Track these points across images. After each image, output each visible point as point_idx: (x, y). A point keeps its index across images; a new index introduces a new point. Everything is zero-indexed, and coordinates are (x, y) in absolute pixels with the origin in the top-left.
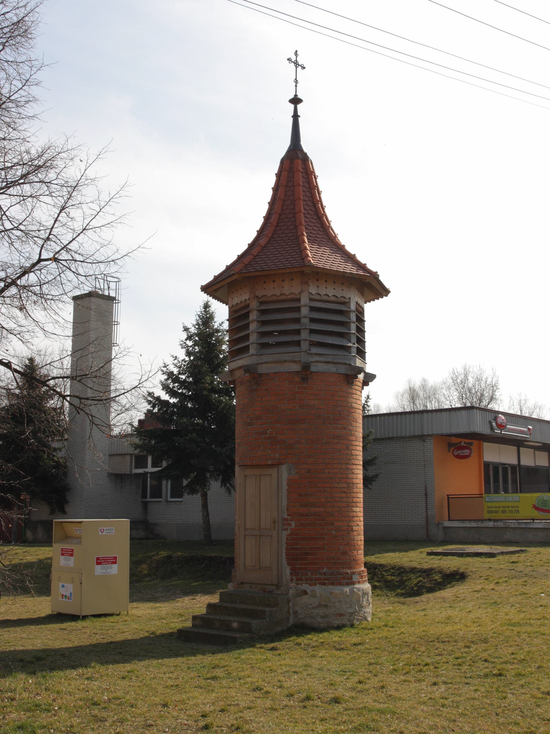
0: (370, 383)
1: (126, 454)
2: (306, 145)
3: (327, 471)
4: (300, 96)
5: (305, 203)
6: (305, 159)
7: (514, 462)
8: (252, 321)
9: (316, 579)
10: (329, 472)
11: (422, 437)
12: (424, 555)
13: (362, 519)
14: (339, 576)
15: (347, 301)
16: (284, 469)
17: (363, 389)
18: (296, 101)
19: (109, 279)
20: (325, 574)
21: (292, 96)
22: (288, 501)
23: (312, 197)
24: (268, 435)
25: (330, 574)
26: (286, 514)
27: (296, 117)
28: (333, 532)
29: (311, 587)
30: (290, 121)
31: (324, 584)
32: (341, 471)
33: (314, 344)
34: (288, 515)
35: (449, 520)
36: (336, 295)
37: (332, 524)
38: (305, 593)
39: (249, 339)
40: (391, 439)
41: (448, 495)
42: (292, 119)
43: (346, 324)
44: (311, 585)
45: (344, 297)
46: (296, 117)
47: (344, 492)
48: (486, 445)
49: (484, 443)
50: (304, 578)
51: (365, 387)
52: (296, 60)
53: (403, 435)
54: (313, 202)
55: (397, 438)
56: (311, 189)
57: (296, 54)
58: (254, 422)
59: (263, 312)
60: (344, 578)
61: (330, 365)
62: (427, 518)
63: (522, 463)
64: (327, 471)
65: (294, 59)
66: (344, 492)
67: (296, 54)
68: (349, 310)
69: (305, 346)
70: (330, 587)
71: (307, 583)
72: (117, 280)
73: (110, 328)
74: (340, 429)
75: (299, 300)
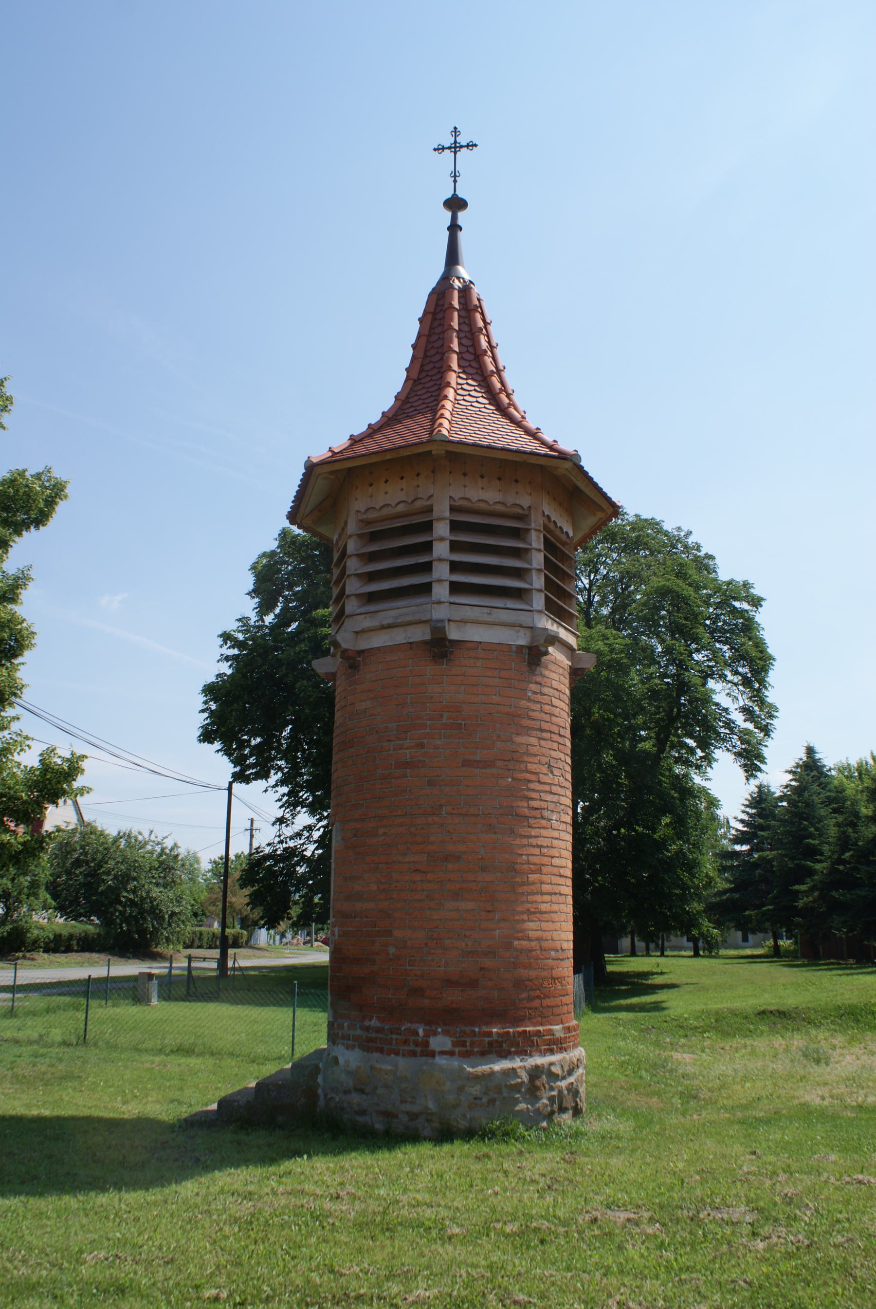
3: (381, 831)
4: (461, 194)
6: (470, 307)
10: (385, 833)
14: (394, 1037)
18: (455, 204)
21: (449, 195)
23: (481, 367)
27: (454, 228)
28: (392, 950)
30: (444, 236)
36: (467, 496)
37: (389, 933)
39: (431, 549)
42: (448, 233)
45: (469, 500)
46: (454, 228)
54: (475, 354)
59: (455, 526)
60: (406, 1042)
67: (471, 146)
69: (441, 591)
70: (376, 1055)
75: (429, 510)
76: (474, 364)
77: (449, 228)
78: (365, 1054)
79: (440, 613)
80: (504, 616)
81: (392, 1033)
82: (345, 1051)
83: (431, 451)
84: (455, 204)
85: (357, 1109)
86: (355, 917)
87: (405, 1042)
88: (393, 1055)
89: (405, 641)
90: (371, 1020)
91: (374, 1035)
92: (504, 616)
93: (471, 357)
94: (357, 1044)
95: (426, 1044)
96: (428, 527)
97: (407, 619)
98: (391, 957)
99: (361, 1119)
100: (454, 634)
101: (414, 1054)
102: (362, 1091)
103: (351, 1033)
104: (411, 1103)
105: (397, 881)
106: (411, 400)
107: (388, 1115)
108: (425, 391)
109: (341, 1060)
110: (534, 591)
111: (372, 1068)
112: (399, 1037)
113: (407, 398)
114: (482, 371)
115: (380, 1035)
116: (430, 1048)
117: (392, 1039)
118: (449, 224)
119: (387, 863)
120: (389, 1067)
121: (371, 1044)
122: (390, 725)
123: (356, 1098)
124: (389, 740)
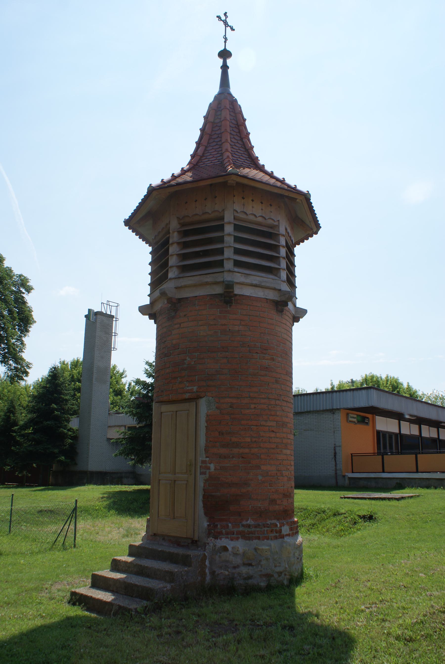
0: (300, 319)
1: (121, 426)
2: (235, 90)
3: (252, 406)
5: (231, 129)
7: (397, 431)
8: (172, 244)
9: (239, 533)
11: (332, 411)
12: (338, 499)
13: (293, 463)
14: (266, 529)
15: (276, 223)
16: (203, 403)
17: (293, 325)
19: (111, 304)
20: (249, 526)
21: (223, 48)
22: (206, 441)
23: (239, 132)
24: (185, 366)
25: (256, 527)
26: (204, 456)
27: (225, 68)
28: (260, 478)
29: (232, 542)
31: (249, 539)
32: (270, 407)
33: (237, 264)
34: (207, 457)
35: (353, 472)
38: (225, 549)
40: (309, 412)
41: (351, 454)
43: (276, 248)
44: (232, 540)
46: (225, 68)
47: (273, 431)
48: (378, 418)
49: (377, 417)
50: (224, 531)
51: (295, 323)
52: (226, 20)
53: (318, 409)
54: (240, 137)
55: (313, 411)
56: (238, 126)
57: (225, 14)
58: (171, 352)
60: (272, 531)
61: (257, 289)
62: (336, 470)
63: (402, 432)
64: (252, 406)
65: (223, 18)
66: (273, 431)
68: (278, 233)
69: (228, 265)
70: (255, 541)
71: (228, 538)
72: (116, 305)
73: (110, 337)
74: (267, 359)
75: (222, 218)
76: (240, 142)
77: (221, 67)
78: (247, 542)
79: (228, 277)
80: (209, 279)
81: (264, 527)
82: (230, 542)
83: (297, 199)
84: (225, 54)
85: (246, 576)
86: (233, 457)
87: (271, 531)
88: (265, 540)
89: (263, 297)
90: (247, 521)
91: (253, 529)
92: (209, 279)
93: (239, 138)
94: (240, 536)
95: (280, 531)
96: (221, 228)
97: (268, 285)
98: (260, 482)
99: (250, 582)
100: (237, 291)
101: (276, 538)
102: (250, 565)
103: (235, 530)
104: (279, 566)
105: (262, 437)
106: (205, 155)
107: (268, 576)
108: (213, 150)
109: (230, 548)
110: (281, 270)
111: (256, 549)
112: (268, 529)
113: (203, 154)
114: (245, 146)
115: (258, 529)
116: (282, 534)
117: (264, 530)
118: (222, 65)
119: (257, 426)
120: (267, 548)
121: (251, 535)
122: (257, 344)
123: (244, 570)
124: (257, 353)
